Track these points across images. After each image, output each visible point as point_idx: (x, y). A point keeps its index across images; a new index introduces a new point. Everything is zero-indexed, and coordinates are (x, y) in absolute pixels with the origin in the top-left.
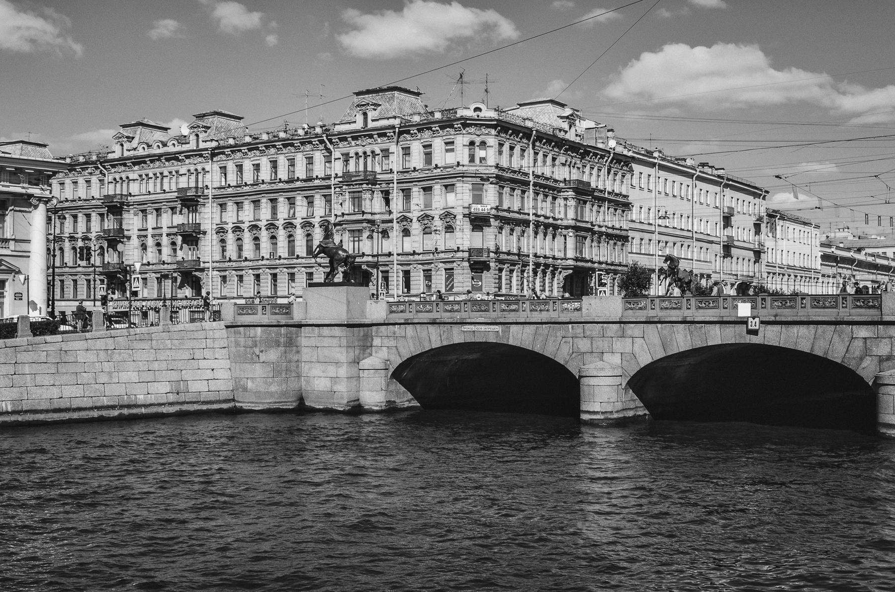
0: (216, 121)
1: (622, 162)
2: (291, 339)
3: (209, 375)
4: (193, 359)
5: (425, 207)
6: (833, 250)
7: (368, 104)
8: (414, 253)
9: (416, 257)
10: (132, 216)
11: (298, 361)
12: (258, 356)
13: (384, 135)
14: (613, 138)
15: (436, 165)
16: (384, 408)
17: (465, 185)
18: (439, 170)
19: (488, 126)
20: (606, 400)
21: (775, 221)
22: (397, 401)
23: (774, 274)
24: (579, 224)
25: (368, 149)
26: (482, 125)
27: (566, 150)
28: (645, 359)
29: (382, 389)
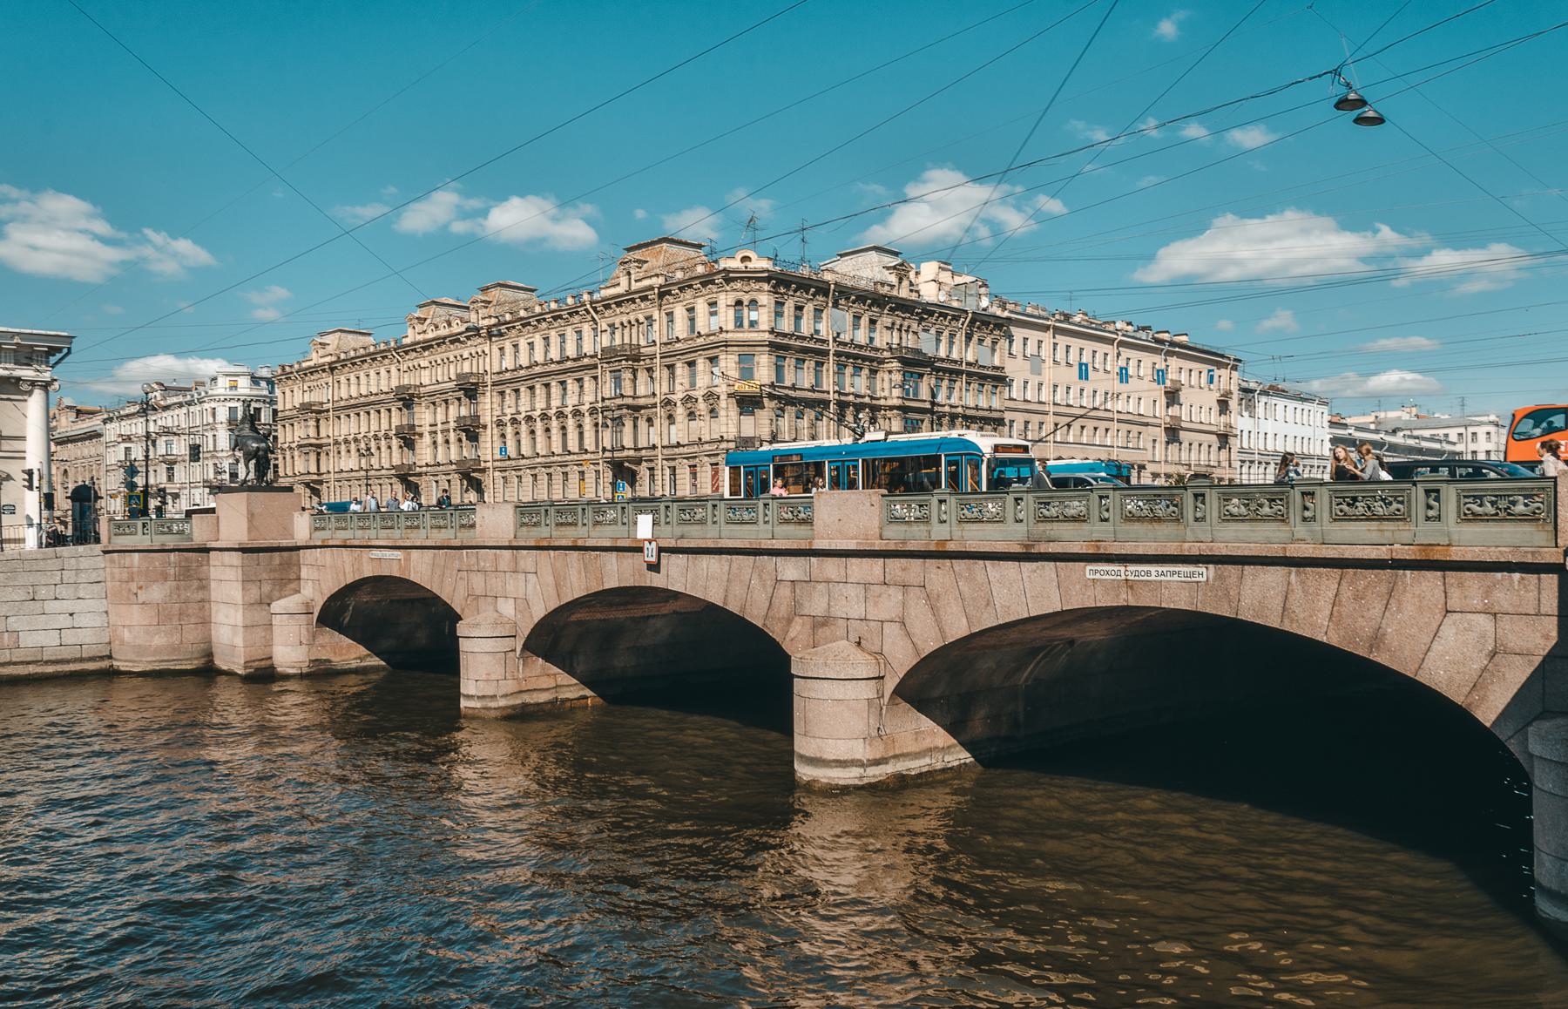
0: (495, 294)
1: (986, 325)
2: (188, 568)
3: (65, 621)
4: (34, 600)
8: (679, 445)
9: (681, 450)
10: (423, 410)
11: (202, 601)
12: (136, 594)
14: (986, 295)
16: (305, 670)
17: (729, 356)
19: (759, 280)
20: (484, 677)
21: (1254, 397)
22: (333, 659)
23: (1252, 462)
24: (908, 404)
26: (750, 279)
27: (891, 309)
29: (301, 643)
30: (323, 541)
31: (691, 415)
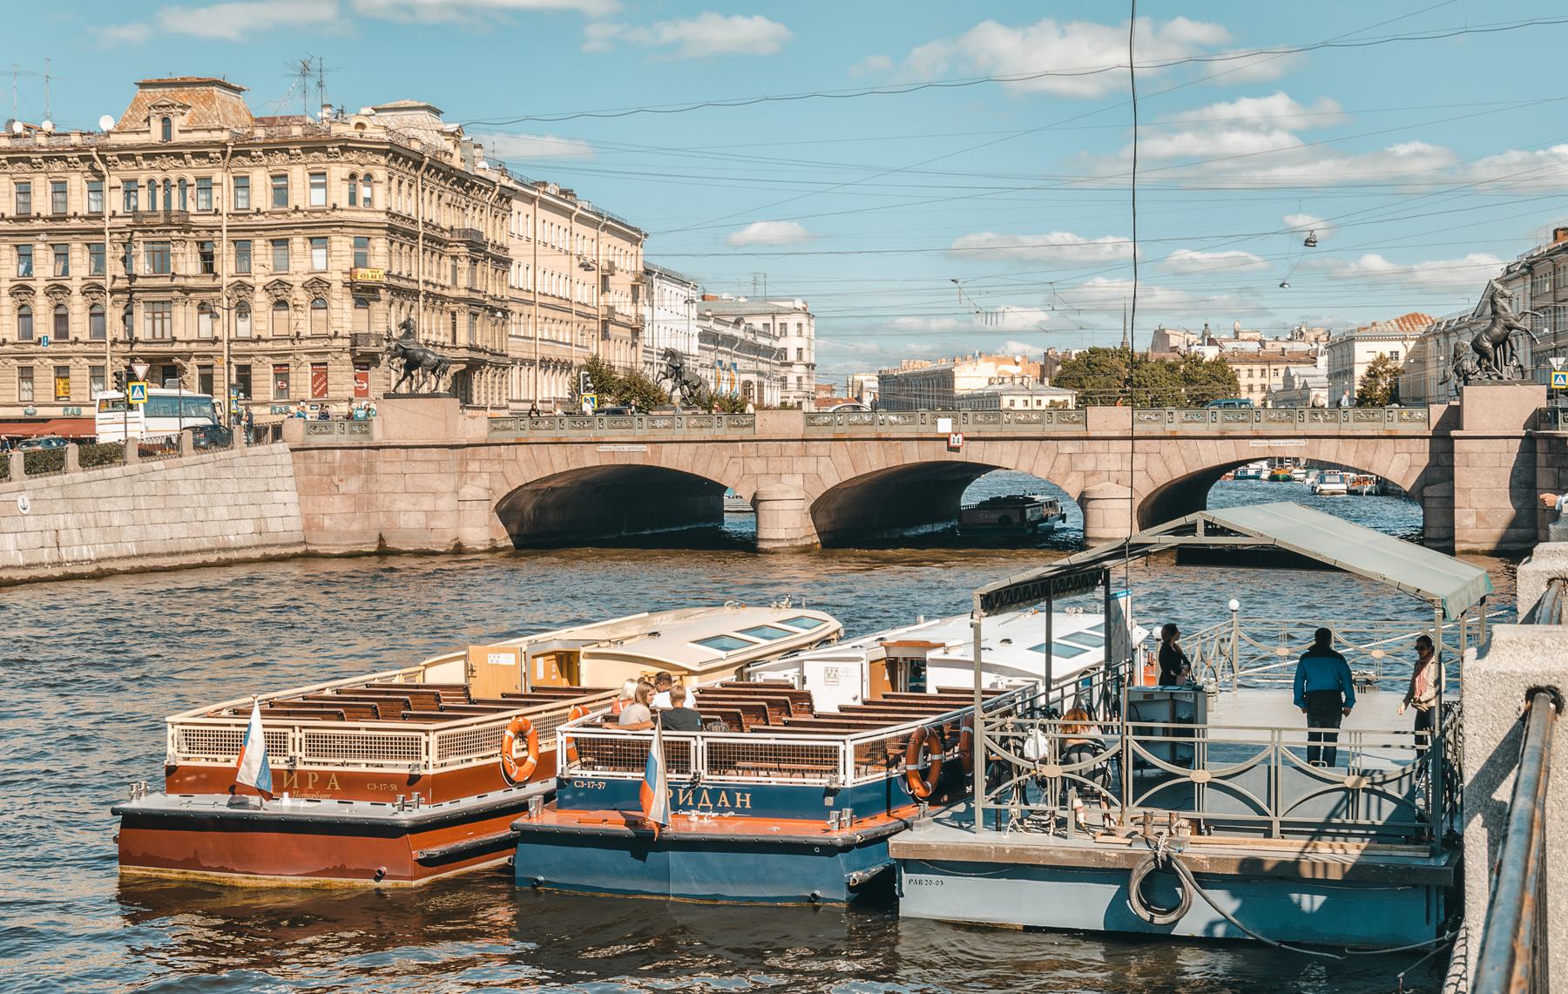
5: (275, 270)
6: (711, 323)
7: (173, 106)
9: (262, 345)
12: (337, 486)
13: (205, 155)
15: (297, 207)
16: (488, 547)
18: (300, 215)
19: (375, 151)
25: (173, 176)
28: (831, 481)
30: (517, 439)
31: (281, 304)
